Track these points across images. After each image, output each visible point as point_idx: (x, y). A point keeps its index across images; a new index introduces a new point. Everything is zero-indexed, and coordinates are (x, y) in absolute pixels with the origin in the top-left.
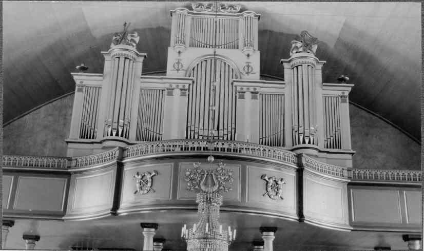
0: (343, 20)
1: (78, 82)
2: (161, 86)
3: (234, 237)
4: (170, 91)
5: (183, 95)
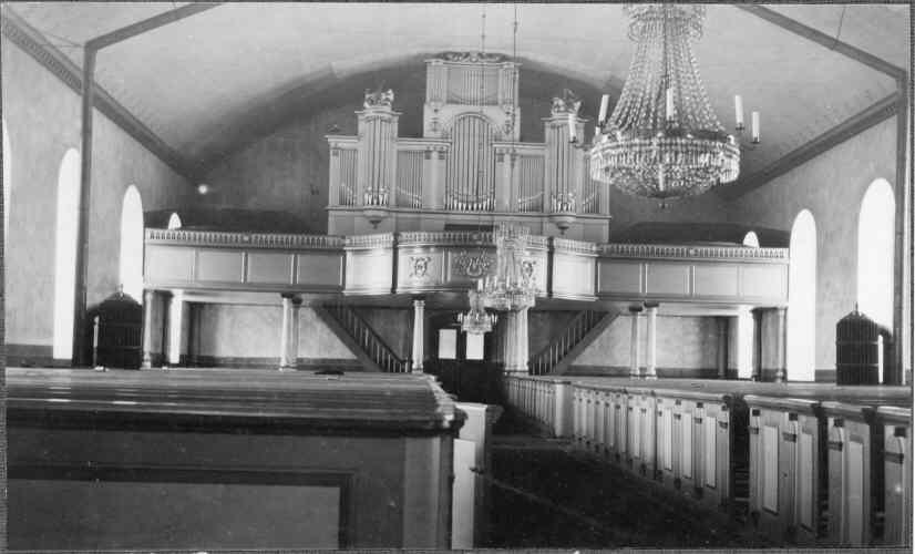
0: (608, 73)
1: (332, 145)
2: (417, 148)
3: (449, 279)
4: (428, 153)
5: (441, 158)
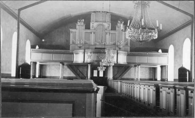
0: (130, 15)
1: (71, 31)
2: (89, 31)
3: (96, 59)
4: (91, 33)
5: (94, 34)
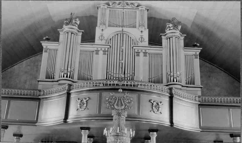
0: (196, 11)
1: (44, 47)
2: (92, 49)
3: (134, 135)
4: (97, 52)
5: (104, 54)
